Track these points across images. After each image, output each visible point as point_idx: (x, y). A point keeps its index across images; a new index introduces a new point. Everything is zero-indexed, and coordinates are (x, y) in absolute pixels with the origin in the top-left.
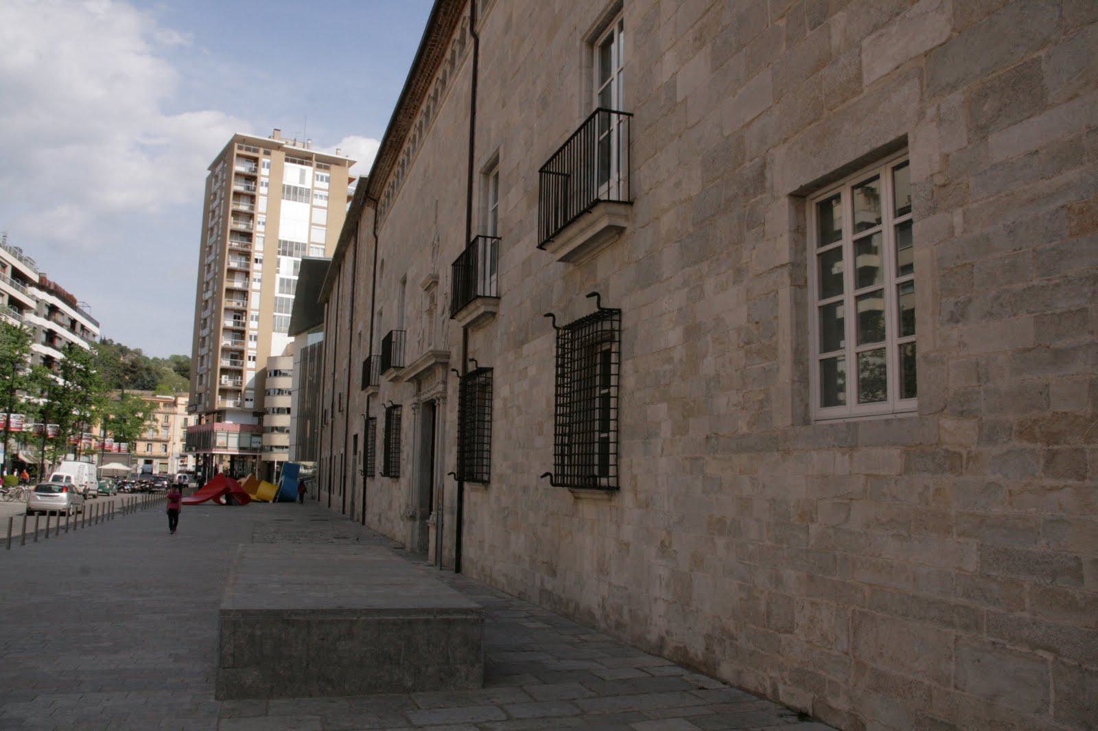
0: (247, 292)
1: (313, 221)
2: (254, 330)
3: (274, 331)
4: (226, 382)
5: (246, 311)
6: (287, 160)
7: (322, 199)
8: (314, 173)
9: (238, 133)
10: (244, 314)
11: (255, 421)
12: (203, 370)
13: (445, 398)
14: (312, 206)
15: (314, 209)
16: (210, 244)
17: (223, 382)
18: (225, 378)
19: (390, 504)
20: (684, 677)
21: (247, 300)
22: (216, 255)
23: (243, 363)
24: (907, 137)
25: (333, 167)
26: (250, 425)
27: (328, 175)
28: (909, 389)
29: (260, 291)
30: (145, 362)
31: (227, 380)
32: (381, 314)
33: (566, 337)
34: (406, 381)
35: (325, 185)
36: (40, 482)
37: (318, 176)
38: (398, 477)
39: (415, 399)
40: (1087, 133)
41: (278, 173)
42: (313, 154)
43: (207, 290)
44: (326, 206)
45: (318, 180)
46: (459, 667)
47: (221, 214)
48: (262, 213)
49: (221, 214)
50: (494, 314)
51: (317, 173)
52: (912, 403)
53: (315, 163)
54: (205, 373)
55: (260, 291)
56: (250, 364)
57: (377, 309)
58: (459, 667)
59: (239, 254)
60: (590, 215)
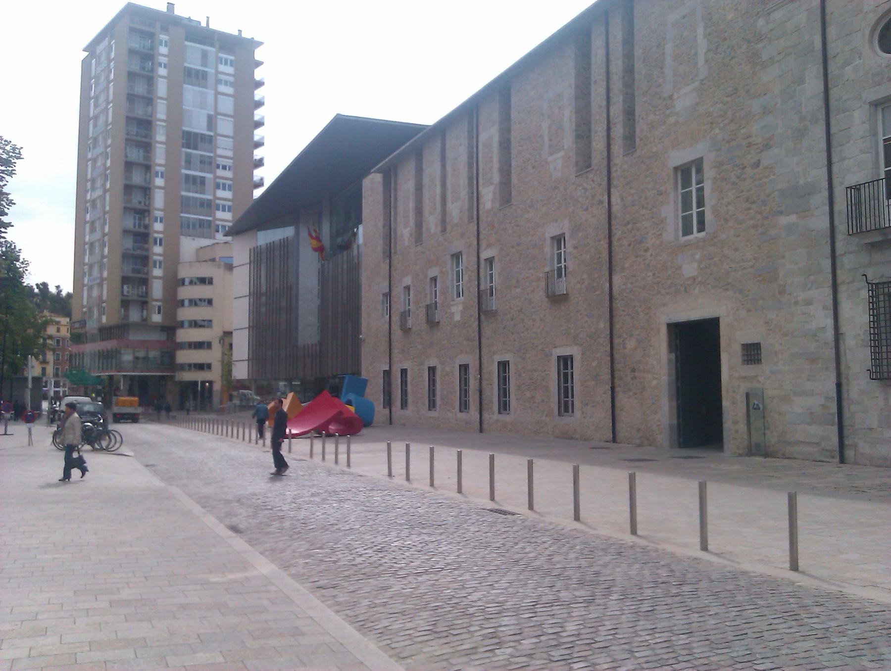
0: (149, 189)
2: (159, 232)
3: (182, 234)
4: (128, 292)
5: (148, 211)
7: (227, 85)
8: (217, 56)
10: (147, 214)
11: (163, 337)
12: (94, 280)
17: (125, 293)
18: (128, 288)
20: (544, 599)
21: (149, 198)
22: (106, 147)
23: (148, 271)
24: (702, 162)
27: (232, 58)
28: (701, 228)
30: (387, 235)
31: (130, 290)
34: (485, 250)
35: (230, 70)
37: (221, 59)
40: (184, 667)
43: (93, 189)
45: (221, 63)
51: (221, 55)
52: (702, 234)
56: (157, 272)
59: (137, 146)
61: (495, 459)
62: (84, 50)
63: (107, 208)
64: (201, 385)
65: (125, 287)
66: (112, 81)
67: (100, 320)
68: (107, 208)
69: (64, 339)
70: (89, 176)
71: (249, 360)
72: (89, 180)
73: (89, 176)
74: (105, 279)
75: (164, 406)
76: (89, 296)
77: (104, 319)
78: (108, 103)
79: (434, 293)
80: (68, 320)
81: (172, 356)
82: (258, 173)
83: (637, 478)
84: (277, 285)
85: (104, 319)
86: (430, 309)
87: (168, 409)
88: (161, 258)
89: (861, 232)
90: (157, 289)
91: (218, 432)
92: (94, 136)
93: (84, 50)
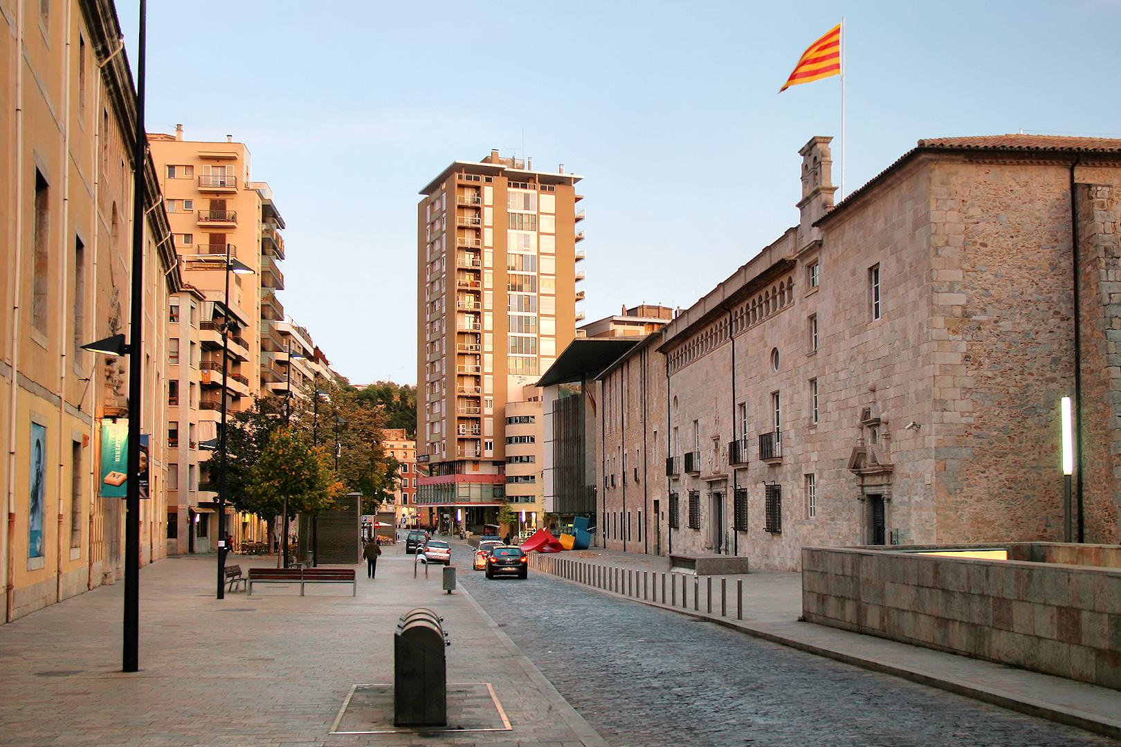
1: (541, 251)
6: (509, 185)
9: (457, 161)
13: (726, 494)
14: (539, 234)
15: (541, 236)
16: (432, 201)
19: (694, 542)
25: (557, 187)
26: (491, 475)
29: (492, 353)
32: (676, 429)
33: (981, 385)
36: (315, 566)
38: (699, 529)
39: (709, 491)
41: (501, 201)
42: (535, 174)
44: (554, 314)
46: (928, 476)
47: (444, 208)
48: (488, 268)
49: (444, 208)
50: (746, 469)
53: (539, 186)
54: (438, 340)
55: (492, 353)
57: (673, 425)
58: (928, 476)
60: (996, 145)
61: (743, 585)
62: (422, 192)
63: (444, 352)
64: (1057, 432)
65: (461, 426)
66: (444, 294)
67: (441, 454)
68: (444, 352)
69: (411, 464)
70: (428, 221)
71: (554, 496)
72: (428, 322)
73: (428, 221)
74: (444, 418)
75: (1076, 552)
76: (432, 432)
77: (444, 456)
78: (443, 213)
79: (743, 424)
80: (414, 443)
81: (503, 489)
82: (579, 308)
83: (713, 581)
84: (571, 435)
85: (444, 456)
86: (689, 457)
87: (945, 562)
88: (491, 398)
89: (768, 458)
90: (488, 427)
91: (594, 569)
92: (432, 241)
93: (422, 192)
